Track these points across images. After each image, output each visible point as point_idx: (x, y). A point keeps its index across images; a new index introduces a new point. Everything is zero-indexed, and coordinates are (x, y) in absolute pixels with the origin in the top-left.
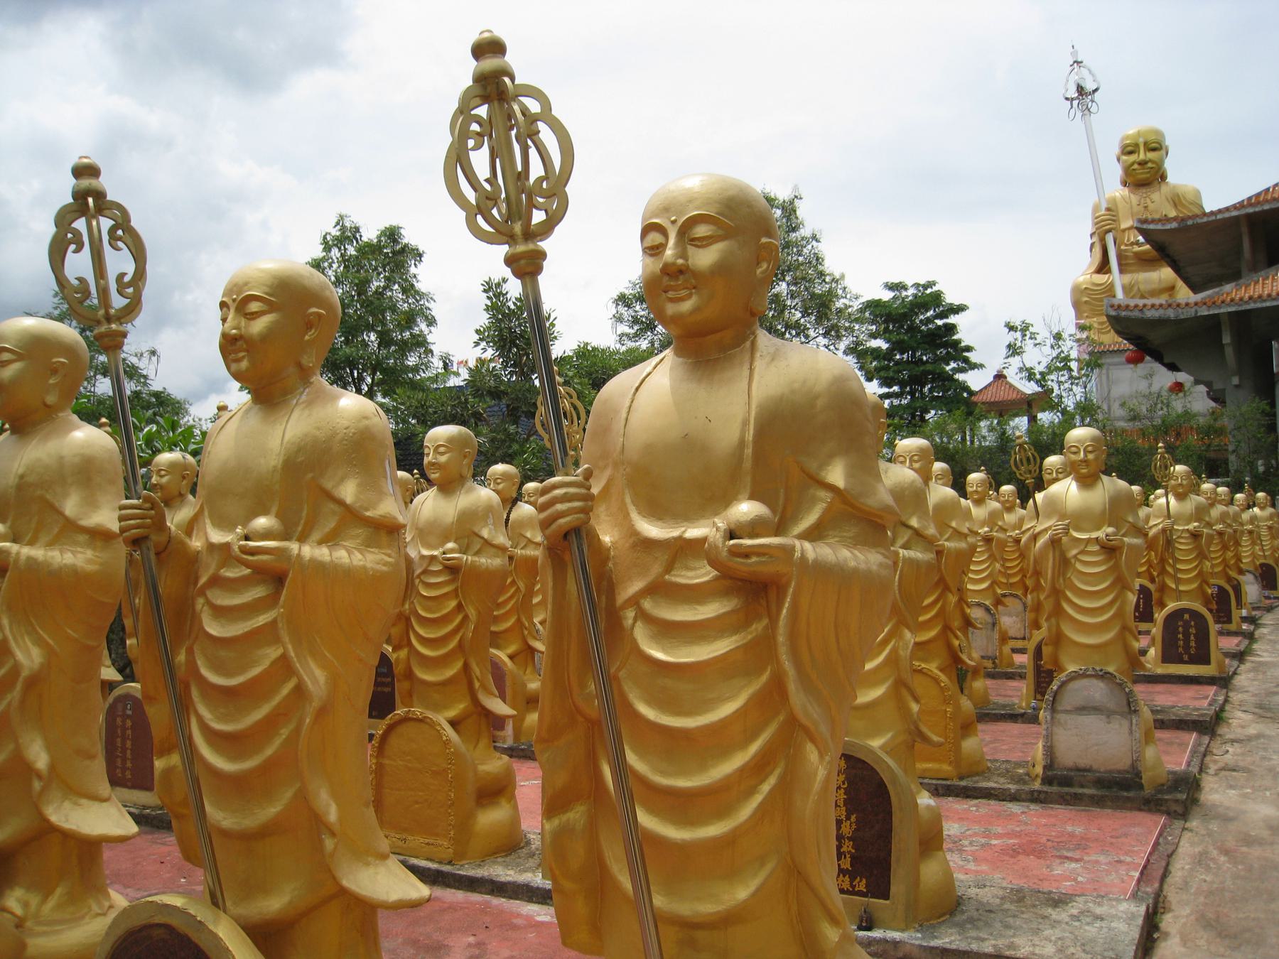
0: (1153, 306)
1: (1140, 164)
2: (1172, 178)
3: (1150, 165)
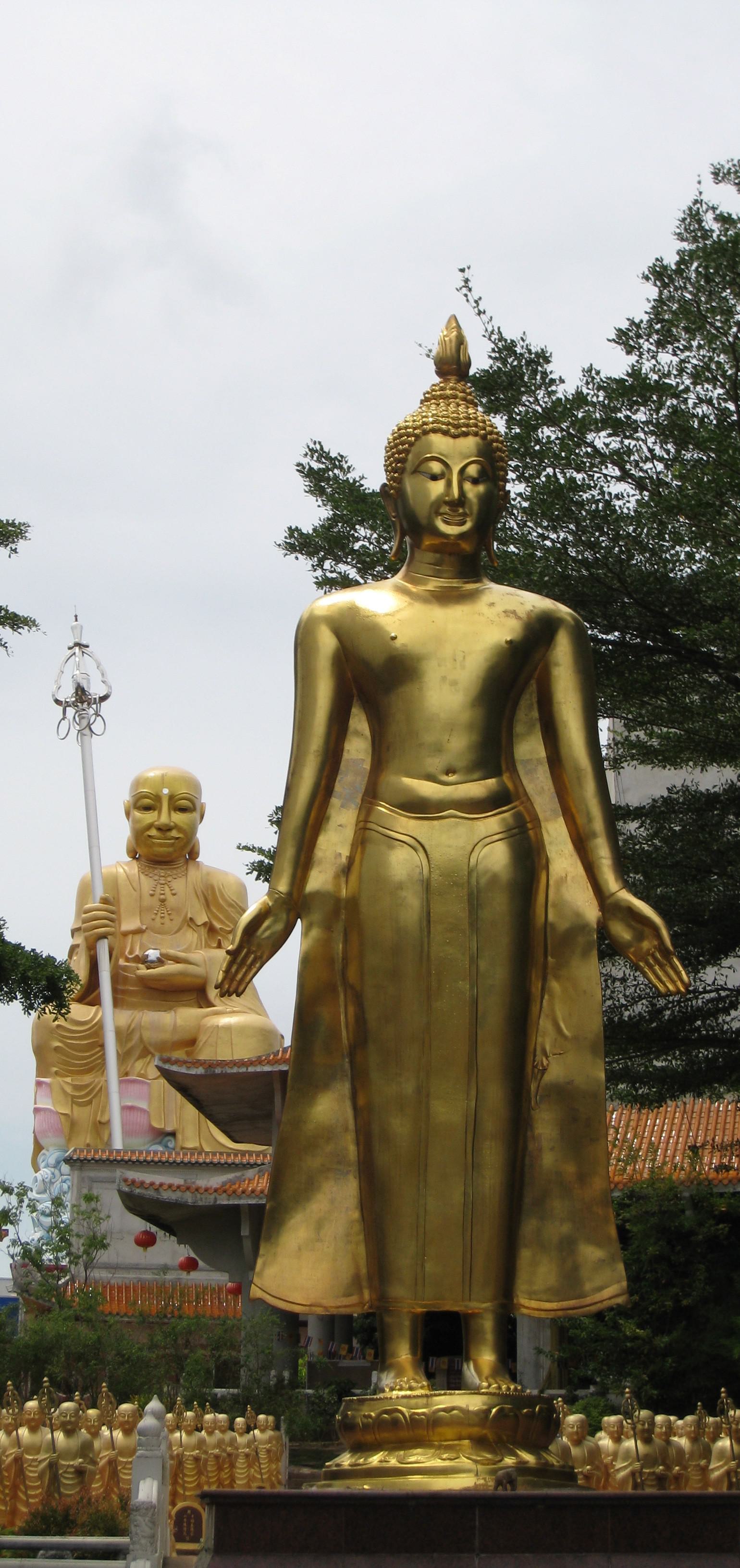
0: (170, 1186)
1: (159, 829)
2: (204, 857)
3: (174, 833)
